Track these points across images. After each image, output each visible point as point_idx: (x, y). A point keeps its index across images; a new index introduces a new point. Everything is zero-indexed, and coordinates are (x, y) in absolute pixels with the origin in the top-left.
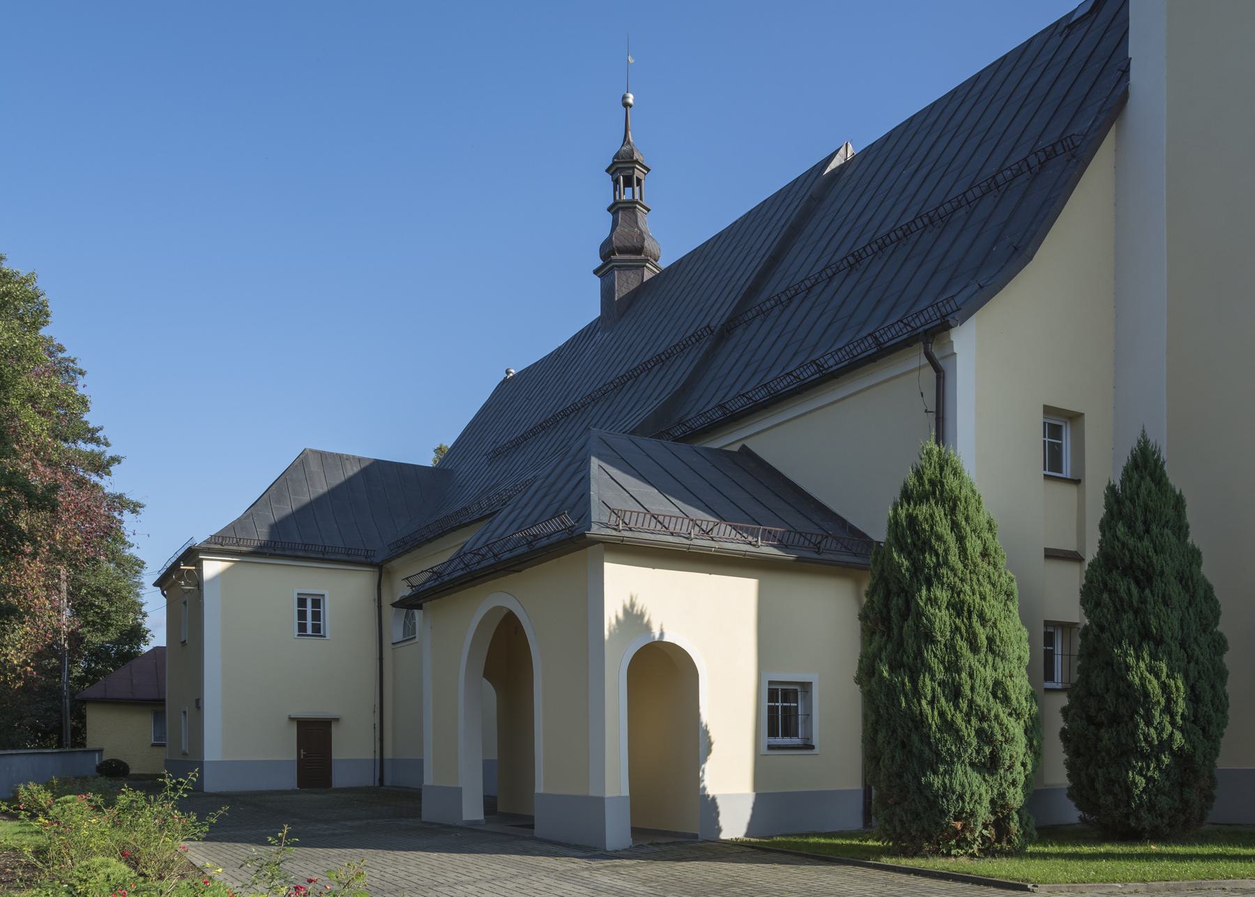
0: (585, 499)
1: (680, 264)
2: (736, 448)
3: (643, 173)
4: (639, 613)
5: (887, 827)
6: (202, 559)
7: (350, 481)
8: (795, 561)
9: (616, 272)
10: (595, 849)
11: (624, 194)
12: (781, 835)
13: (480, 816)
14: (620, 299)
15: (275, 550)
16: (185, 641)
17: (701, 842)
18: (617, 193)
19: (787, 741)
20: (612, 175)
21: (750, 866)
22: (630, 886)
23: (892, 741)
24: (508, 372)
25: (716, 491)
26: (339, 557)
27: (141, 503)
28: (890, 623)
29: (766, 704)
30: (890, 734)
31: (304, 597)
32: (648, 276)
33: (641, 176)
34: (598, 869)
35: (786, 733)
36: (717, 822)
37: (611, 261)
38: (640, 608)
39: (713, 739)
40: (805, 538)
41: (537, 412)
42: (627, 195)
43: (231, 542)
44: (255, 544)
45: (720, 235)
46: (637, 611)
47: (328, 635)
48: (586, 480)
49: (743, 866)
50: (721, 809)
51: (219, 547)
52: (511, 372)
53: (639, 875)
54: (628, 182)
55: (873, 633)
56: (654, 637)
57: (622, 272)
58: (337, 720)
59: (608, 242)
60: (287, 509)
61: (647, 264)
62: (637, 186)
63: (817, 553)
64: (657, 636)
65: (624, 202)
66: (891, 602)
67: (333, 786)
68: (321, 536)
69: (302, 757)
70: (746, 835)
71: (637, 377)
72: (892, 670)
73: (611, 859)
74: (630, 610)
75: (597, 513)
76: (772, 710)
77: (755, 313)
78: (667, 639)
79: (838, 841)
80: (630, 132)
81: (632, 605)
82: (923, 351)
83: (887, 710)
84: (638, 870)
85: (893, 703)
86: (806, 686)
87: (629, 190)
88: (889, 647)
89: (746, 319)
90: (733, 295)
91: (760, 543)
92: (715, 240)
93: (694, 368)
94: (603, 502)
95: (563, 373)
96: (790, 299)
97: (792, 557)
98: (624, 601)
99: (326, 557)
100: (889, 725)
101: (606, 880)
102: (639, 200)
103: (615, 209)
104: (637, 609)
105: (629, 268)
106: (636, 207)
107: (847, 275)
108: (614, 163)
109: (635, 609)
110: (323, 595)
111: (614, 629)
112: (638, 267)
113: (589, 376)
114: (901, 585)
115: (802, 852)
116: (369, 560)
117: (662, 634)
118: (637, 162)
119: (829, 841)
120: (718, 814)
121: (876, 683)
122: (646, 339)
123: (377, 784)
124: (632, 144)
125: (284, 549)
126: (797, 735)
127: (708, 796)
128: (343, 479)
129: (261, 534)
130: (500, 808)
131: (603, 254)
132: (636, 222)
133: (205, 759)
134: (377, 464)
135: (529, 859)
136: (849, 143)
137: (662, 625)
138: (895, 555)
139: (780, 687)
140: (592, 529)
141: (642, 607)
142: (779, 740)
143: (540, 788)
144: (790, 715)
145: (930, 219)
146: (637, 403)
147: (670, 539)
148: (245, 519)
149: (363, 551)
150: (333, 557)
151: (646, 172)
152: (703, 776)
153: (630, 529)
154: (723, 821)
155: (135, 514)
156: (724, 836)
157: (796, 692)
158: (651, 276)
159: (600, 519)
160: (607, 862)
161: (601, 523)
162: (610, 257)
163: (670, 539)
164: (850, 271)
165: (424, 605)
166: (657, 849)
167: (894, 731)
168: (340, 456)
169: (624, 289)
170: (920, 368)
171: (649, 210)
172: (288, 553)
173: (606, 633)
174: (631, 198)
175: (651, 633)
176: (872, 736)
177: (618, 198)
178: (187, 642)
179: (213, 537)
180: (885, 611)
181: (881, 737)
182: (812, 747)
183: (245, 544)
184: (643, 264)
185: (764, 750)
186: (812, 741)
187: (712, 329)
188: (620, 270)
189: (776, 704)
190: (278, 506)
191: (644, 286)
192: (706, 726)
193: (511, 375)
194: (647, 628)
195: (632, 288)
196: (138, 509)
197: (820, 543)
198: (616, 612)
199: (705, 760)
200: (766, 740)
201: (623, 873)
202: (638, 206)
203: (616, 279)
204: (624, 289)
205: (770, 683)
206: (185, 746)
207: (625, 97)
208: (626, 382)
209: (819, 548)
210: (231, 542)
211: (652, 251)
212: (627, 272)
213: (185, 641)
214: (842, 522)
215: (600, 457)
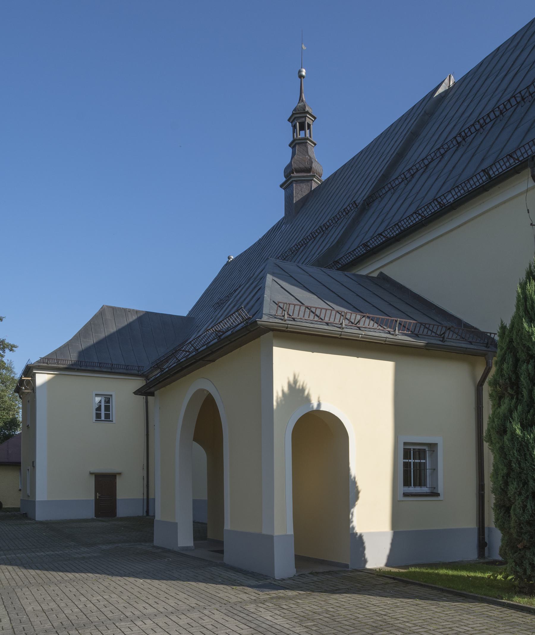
0: (260, 300)
1: (335, 175)
2: (375, 275)
3: (312, 120)
4: (301, 387)
5: (518, 569)
6: (35, 373)
7: (130, 325)
8: (425, 346)
9: (294, 185)
10: (266, 577)
11: (299, 135)
12: (415, 566)
13: (190, 543)
14: (297, 202)
15: (81, 367)
16: (28, 425)
17: (351, 572)
18: (295, 134)
19: (418, 490)
20: (292, 122)
21: (395, 601)
22: (287, 626)
23: (523, 492)
24: (229, 258)
25: (361, 299)
26: (121, 371)
27: (15, 345)
28: (518, 387)
29: (401, 461)
30: (521, 486)
31: (108, 397)
32: (314, 186)
33: (311, 122)
34: (264, 602)
35: (420, 485)
36: (363, 555)
37: (291, 177)
38: (301, 384)
39: (360, 488)
40: (432, 331)
41: (244, 278)
42: (302, 135)
43: (53, 362)
44: (69, 363)
45: (362, 152)
46: (299, 386)
47: (114, 422)
48: (262, 289)
49: (389, 601)
50: (367, 545)
51: (46, 365)
52: (231, 258)
53: (298, 611)
54: (302, 128)
55: (501, 397)
56: (313, 407)
57: (298, 184)
58: (120, 474)
59: (290, 165)
60: (91, 341)
61: (314, 179)
62: (308, 129)
63: (442, 341)
64: (315, 406)
65: (300, 139)
66: (520, 368)
67: (117, 516)
68: (111, 358)
69: (98, 498)
70: (387, 565)
71: (306, 244)
72: (523, 427)
73: (277, 589)
74: (294, 386)
75: (268, 308)
76: (406, 466)
77: (387, 189)
78: (323, 408)
79: (464, 573)
80: (303, 94)
81: (295, 382)
82: (530, 175)
83: (519, 464)
84: (297, 604)
85: (525, 457)
86: (433, 447)
87: (302, 132)
88: (519, 408)
89: (381, 194)
90: (370, 183)
91: (397, 332)
92: (358, 156)
93: (344, 232)
94: (274, 302)
95: (261, 253)
96: (413, 176)
97: (421, 343)
98: (288, 378)
99: (113, 371)
100: (520, 477)
101: (267, 616)
102: (309, 137)
103: (294, 144)
104: (300, 384)
105: (302, 181)
106: (307, 142)
107: (456, 150)
108: (293, 114)
109: (298, 384)
110: (111, 395)
111: (281, 401)
112: (308, 181)
113: (277, 251)
114: (530, 352)
115: (437, 586)
116: (140, 373)
117: (319, 405)
118: (308, 112)
119: (455, 573)
120: (364, 548)
121: (508, 440)
122: (313, 222)
123: (145, 514)
124: (304, 102)
125: (86, 366)
126: (425, 485)
127: (356, 533)
128: (126, 323)
129: (73, 357)
130: (210, 535)
131: (286, 174)
132: (307, 152)
133: (37, 500)
134: (147, 313)
135: (211, 588)
136: (451, 75)
137: (319, 398)
138: (525, 325)
139: (412, 447)
140: (262, 319)
141: (303, 383)
142: (412, 489)
143: (228, 526)
144: (420, 469)
145: (522, 97)
146: (306, 259)
147: (326, 327)
148: (63, 348)
149: (136, 367)
150: (117, 371)
151: (314, 120)
152: (352, 518)
153: (294, 319)
154: (369, 554)
155: (12, 352)
156: (369, 566)
157: (424, 451)
158: (316, 186)
159: (270, 312)
160: (274, 593)
161: (271, 315)
162: (290, 175)
163: (326, 327)
164: (458, 147)
165: (155, 392)
166: (315, 579)
167: (525, 483)
168: (125, 310)
169: (299, 196)
170: (527, 191)
171: (315, 144)
172: (89, 368)
173: (275, 403)
174: (304, 136)
175: (311, 404)
176: (502, 487)
177: (295, 137)
178: (29, 426)
179: (42, 359)
180: (513, 377)
181: (512, 488)
182: (438, 495)
183: (62, 363)
184: (312, 178)
185: (400, 497)
186: (438, 490)
187: (357, 204)
188: (297, 183)
189: (410, 461)
190: (85, 340)
191: (312, 193)
192: (355, 478)
193: (231, 259)
194: (308, 400)
195: (304, 194)
196: (14, 349)
197: (444, 333)
198: (282, 387)
199: (354, 505)
200: (402, 489)
201: (284, 607)
202: (308, 141)
203: (294, 189)
204: (299, 196)
205: (405, 444)
206: (28, 492)
207: (300, 71)
208: (299, 249)
209: (443, 338)
210: (53, 362)
211: (317, 170)
212: (302, 184)
213: (28, 425)
214: (459, 322)
215: (273, 274)
